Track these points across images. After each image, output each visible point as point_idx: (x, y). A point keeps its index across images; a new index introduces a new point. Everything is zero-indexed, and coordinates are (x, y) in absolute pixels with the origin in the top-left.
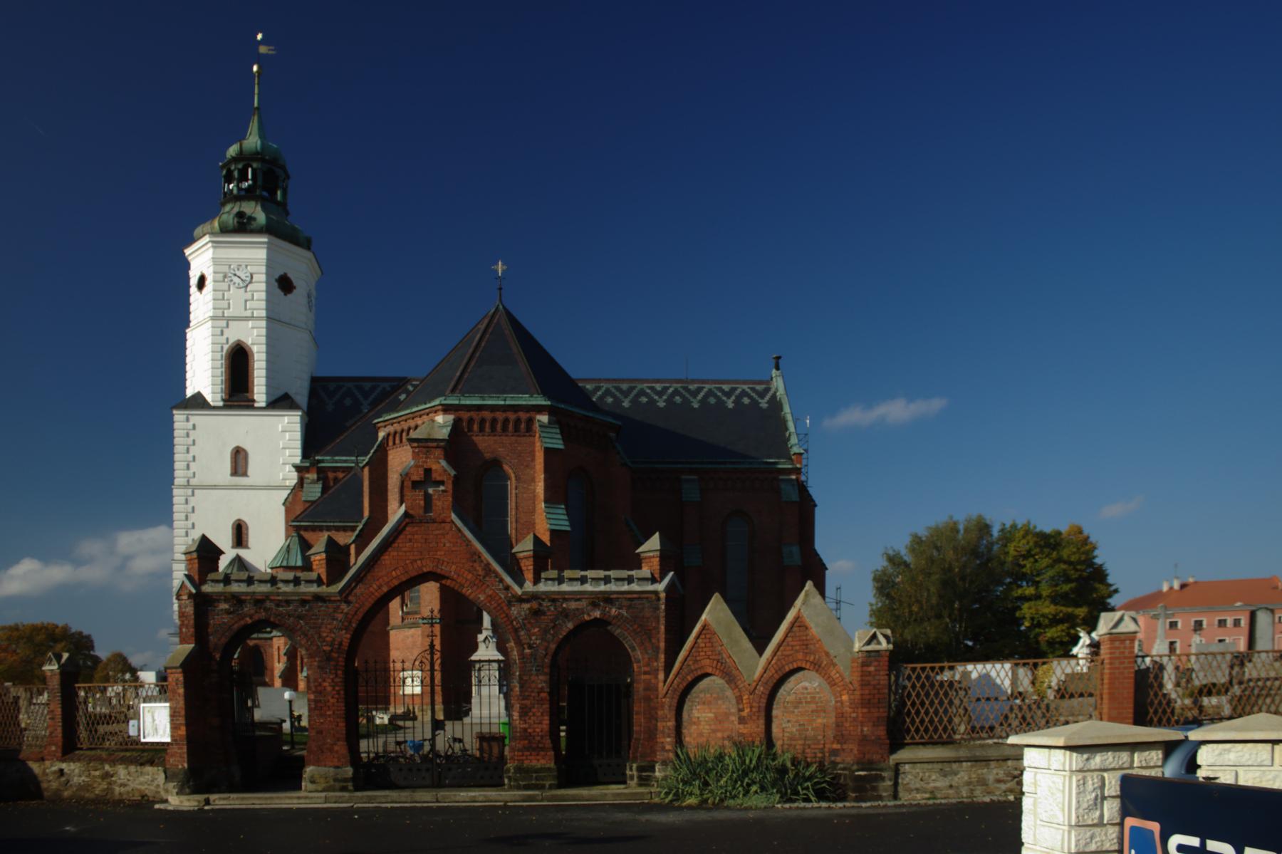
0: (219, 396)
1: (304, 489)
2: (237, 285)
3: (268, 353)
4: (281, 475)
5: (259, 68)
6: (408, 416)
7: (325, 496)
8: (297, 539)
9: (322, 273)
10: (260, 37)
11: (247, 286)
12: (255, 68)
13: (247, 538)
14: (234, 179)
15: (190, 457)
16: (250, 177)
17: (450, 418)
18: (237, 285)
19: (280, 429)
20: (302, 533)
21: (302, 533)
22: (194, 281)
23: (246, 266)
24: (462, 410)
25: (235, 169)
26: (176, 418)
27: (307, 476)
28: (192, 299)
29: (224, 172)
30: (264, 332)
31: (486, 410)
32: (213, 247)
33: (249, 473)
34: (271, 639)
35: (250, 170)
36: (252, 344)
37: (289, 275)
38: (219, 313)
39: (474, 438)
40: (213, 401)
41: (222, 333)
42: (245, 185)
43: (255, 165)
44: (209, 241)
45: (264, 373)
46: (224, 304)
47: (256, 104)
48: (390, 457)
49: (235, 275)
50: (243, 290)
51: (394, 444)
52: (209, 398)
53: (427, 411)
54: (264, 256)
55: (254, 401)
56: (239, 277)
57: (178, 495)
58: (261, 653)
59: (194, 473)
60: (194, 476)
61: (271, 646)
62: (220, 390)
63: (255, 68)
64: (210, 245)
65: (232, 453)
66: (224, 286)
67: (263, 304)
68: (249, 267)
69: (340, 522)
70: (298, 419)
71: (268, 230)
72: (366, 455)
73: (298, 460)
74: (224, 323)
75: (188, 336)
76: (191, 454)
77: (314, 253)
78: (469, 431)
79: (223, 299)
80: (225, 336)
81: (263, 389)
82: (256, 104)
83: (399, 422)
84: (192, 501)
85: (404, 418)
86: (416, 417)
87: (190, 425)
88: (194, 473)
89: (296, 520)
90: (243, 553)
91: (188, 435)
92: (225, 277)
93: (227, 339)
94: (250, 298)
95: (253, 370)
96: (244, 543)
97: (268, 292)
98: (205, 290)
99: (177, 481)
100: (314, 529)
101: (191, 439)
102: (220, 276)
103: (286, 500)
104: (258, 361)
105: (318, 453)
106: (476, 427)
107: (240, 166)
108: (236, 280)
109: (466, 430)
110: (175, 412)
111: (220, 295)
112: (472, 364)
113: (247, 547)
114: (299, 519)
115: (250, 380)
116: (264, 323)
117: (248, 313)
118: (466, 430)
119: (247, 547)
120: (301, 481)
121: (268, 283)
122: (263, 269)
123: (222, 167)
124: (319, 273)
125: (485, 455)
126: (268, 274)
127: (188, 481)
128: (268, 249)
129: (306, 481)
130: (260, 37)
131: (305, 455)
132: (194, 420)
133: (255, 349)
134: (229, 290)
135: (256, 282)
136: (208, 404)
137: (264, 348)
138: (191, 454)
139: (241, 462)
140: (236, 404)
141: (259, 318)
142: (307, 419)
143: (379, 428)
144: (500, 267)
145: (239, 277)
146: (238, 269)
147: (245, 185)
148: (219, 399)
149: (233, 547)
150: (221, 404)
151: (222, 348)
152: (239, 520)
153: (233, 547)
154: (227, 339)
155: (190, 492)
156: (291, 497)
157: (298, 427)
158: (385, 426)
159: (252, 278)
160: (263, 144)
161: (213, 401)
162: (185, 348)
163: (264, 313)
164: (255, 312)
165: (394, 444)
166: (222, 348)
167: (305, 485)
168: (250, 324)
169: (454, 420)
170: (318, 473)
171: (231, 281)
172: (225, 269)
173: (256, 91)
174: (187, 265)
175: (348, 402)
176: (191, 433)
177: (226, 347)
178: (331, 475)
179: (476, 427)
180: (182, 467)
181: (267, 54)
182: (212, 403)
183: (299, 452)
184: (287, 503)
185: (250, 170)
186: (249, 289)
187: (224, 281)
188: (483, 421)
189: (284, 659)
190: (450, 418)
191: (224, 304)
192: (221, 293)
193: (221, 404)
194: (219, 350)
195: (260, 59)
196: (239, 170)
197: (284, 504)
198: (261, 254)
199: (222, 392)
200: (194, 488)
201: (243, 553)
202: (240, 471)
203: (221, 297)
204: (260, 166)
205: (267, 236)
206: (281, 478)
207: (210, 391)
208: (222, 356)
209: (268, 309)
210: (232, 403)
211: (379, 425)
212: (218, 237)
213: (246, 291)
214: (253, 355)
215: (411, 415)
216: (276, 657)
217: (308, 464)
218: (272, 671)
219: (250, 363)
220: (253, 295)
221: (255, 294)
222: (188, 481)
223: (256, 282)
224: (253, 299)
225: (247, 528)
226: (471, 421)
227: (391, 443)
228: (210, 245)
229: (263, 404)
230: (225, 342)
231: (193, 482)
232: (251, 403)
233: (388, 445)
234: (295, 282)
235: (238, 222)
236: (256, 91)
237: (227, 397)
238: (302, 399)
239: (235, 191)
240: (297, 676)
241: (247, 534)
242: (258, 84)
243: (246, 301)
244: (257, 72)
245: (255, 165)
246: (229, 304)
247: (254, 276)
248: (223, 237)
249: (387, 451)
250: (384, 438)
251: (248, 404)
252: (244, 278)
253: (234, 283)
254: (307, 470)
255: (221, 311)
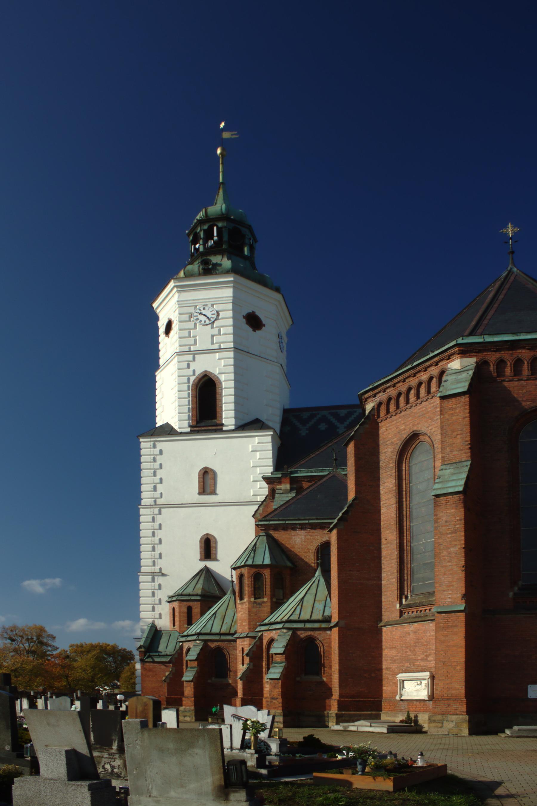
0: (186, 424)
1: (276, 499)
2: (203, 322)
3: (236, 381)
4: (252, 491)
5: (223, 150)
6: (407, 374)
7: (299, 497)
8: (265, 538)
9: (293, 323)
10: (222, 125)
11: (214, 322)
12: (219, 151)
13: (216, 550)
14: (201, 239)
15: (157, 479)
16: (215, 234)
17: (471, 361)
18: (203, 322)
19: (250, 450)
20: (271, 532)
21: (271, 532)
22: (162, 325)
23: (213, 305)
24: (488, 350)
25: (201, 230)
26: (142, 445)
27: (278, 487)
28: (161, 339)
29: (191, 238)
30: (231, 361)
31: (524, 348)
32: (178, 291)
33: (217, 492)
34: (235, 641)
35: (215, 228)
36: (219, 374)
37: (257, 313)
38: (186, 349)
39: (506, 384)
40: (179, 428)
41: (189, 366)
42: (211, 243)
43: (220, 225)
44: (174, 287)
45: (232, 406)
46: (191, 341)
47: (221, 180)
48: (382, 430)
49: (201, 314)
50: (210, 326)
51: (388, 412)
52: (176, 427)
53: (436, 359)
54: (231, 294)
55: (222, 425)
56: (205, 315)
57: (145, 516)
58: (224, 655)
59: (161, 494)
60: (161, 497)
61: (235, 648)
62: (187, 418)
63: (219, 151)
64: (175, 289)
65: (199, 475)
66: (191, 325)
67: (231, 338)
68: (215, 306)
69: (317, 519)
70: (269, 439)
71: (234, 270)
72: (335, 519)
73: (269, 470)
74: (190, 357)
75: (158, 378)
76: (158, 477)
77: (283, 296)
78: (498, 376)
79: (190, 336)
80: (192, 369)
81: (232, 414)
82: (221, 180)
83: (394, 386)
84: (159, 519)
85: (400, 378)
86: (419, 371)
87: (157, 451)
88: (161, 494)
89: (265, 518)
90: (211, 565)
91: (155, 460)
92: (191, 316)
93: (194, 371)
94: (217, 333)
95: (222, 404)
96: (212, 556)
97: (235, 326)
98: (172, 333)
99: (143, 502)
100: (285, 528)
101: (158, 463)
102: (186, 317)
103: (256, 512)
104: (225, 388)
105: (290, 466)
106: (508, 371)
107: (206, 227)
108: (202, 318)
109: (495, 375)
110: (141, 440)
111: (186, 333)
112: (491, 313)
113: (216, 560)
114: (268, 518)
115: (218, 406)
116: (231, 354)
117: (216, 346)
118: (495, 375)
119: (216, 560)
120: (272, 493)
121: (234, 318)
122: (230, 306)
123: (189, 235)
124: (291, 323)
125: (524, 404)
126: (234, 310)
127: (155, 501)
128: (234, 287)
129: (277, 491)
130: (222, 125)
131: (279, 464)
132: (159, 446)
133: (222, 378)
134: (195, 328)
135: (222, 318)
136: (176, 431)
137: (232, 376)
138: (158, 477)
139: (209, 482)
140: (203, 428)
141: (226, 349)
142: (279, 442)
143: (366, 400)
144: (510, 230)
145: (205, 315)
146: (204, 309)
147: (211, 243)
148: (187, 425)
149: (201, 560)
150: (188, 430)
151: (189, 379)
152: (207, 534)
153: (201, 560)
154: (194, 371)
155: (156, 511)
156: (261, 509)
157: (269, 446)
158: (375, 396)
159: (218, 314)
160: (227, 209)
161: (179, 428)
162: (155, 396)
163: (232, 345)
164: (222, 345)
165: (388, 412)
166: (189, 379)
167: (277, 495)
168: (217, 355)
169: (477, 362)
170: (291, 484)
171: (197, 319)
172: (191, 310)
173: (221, 170)
174: (156, 318)
175: (323, 427)
176: (158, 457)
177: (192, 379)
178: (305, 485)
179: (508, 371)
180: (150, 489)
181: (231, 138)
182: (179, 430)
183: (270, 462)
184: (258, 515)
185: (215, 228)
186: (215, 326)
187: (190, 321)
188: (518, 363)
189: (247, 660)
190: (471, 361)
191: (191, 341)
192: (188, 331)
193: (188, 430)
194: (186, 381)
195: (223, 143)
196: (205, 231)
197: (253, 516)
198: (228, 293)
199: (189, 419)
200: (161, 507)
201: (211, 565)
202: (208, 490)
203: (187, 335)
204: (225, 224)
205: (233, 275)
206: (252, 494)
207: (177, 419)
208: (189, 386)
209: (235, 342)
210: (200, 429)
211: (366, 396)
212: (183, 281)
213: (212, 328)
214: (221, 383)
215: (412, 372)
216: (240, 659)
217: (280, 476)
218: (236, 672)
219: (218, 391)
220: (220, 330)
221: (222, 329)
222: (155, 501)
223: (222, 318)
224: (219, 334)
225: (216, 542)
226: (501, 363)
227: (383, 413)
228: (175, 289)
229: (233, 428)
230: (192, 374)
231: (159, 502)
232: (219, 427)
233: (379, 416)
234: (264, 321)
235: (203, 269)
236: (221, 170)
237: (195, 423)
238: (276, 421)
239: (201, 249)
240: (262, 678)
241: (216, 548)
242: (222, 163)
243: (213, 336)
244: (221, 153)
245: (220, 225)
246: (195, 340)
247: (221, 313)
248: (187, 281)
249: (377, 424)
250: (373, 409)
251: (190, 337)
252: (209, 316)
253: (201, 321)
254: (279, 481)
255: (188, 347)
